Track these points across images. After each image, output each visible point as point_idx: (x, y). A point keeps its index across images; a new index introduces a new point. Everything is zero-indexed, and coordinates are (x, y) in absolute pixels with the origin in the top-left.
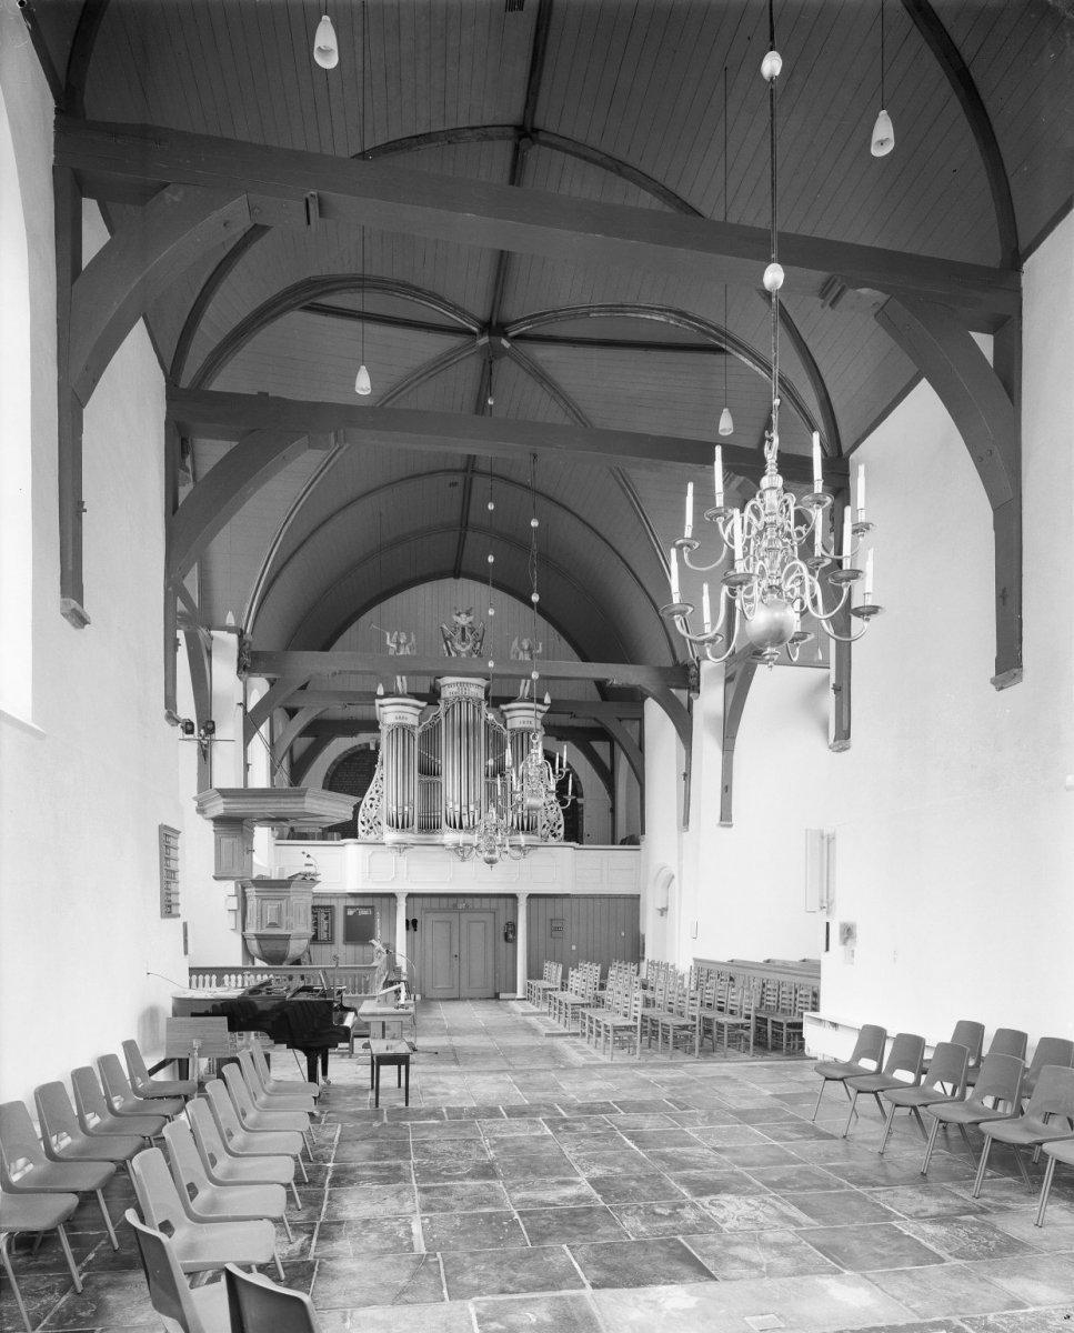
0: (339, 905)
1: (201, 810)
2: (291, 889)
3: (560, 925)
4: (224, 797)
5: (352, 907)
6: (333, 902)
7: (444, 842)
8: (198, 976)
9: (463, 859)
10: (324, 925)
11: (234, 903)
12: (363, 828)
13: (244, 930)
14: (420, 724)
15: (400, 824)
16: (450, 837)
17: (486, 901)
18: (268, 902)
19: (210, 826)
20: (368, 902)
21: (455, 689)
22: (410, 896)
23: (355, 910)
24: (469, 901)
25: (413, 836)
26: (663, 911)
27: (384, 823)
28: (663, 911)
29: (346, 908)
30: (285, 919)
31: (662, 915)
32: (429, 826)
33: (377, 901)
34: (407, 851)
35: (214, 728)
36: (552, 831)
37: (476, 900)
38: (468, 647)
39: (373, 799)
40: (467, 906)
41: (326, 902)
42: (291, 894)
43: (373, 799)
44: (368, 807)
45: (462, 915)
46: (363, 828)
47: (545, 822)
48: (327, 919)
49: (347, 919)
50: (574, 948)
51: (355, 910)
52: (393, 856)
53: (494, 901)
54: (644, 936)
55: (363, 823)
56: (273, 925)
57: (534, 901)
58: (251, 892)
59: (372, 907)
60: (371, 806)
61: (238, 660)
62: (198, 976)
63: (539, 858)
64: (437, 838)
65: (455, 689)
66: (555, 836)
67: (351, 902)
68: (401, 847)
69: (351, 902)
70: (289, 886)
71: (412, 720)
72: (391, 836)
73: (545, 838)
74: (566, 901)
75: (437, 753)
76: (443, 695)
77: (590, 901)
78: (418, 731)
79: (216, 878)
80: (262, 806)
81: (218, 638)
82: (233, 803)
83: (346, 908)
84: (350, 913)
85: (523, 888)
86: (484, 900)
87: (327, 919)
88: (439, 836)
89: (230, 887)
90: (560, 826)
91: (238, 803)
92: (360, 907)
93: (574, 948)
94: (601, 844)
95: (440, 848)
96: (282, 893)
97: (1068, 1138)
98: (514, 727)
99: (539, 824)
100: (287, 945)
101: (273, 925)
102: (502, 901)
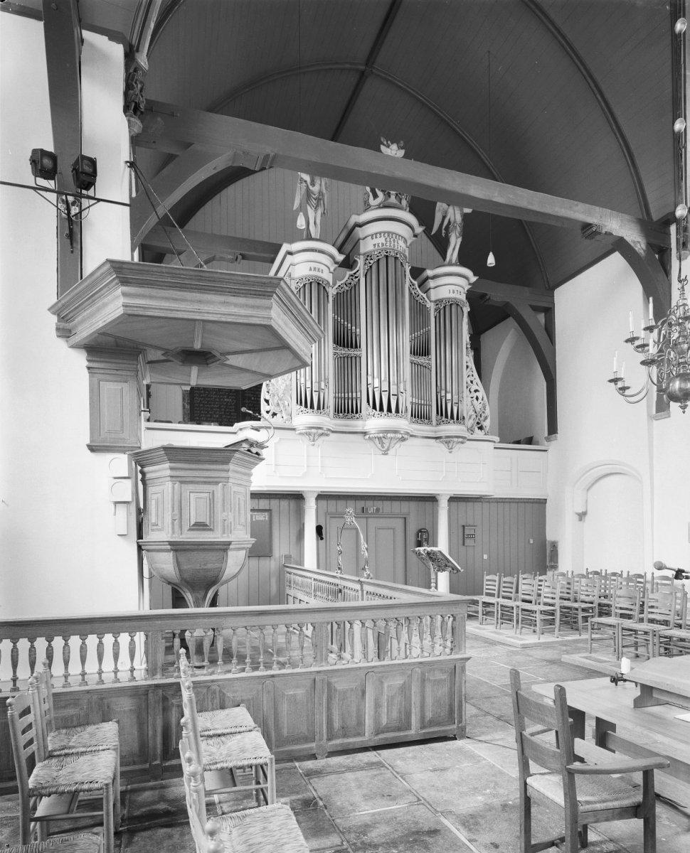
1: (65, 332)
2: (231, 466)
3: (473, 533)
4: (124, 282)
7: (366, 429)
8: (84, 637)
9: (385, 453)
11: (125, 491)
12: (268, 408)
13: (140, 536)
16: (374, 422)
17: (396, 504)
18: (191, 487)
19: (80, 360)
21: (381, 240)
24: (379, 504)
25: (328, 419)
26: (582, 516)
28: (582, 516)
30: (220, 516)
31: (581, 520)
32: (346, 409)
33: (275, 503)
35: (94, 174)
36: (478, 423)
37: (387, 503)
40: (378, 510)
42: (230, 474)
45: (370, 520)
50: (485, 557)
53: (405, 505)
54: (554, 545)
55: (267, 401)
56: (200, 526)
57: (454, 504)
58: (160, 471)
59: (269, 511)
61: (126, 94)
62: (84, 637)
63: (465, 452)
64: (358, 425)
65: (381, 240)
66: (481, 428)
68: (315, 433)
70: (226, 462)
71: (327, 276)
73: (471, 430)
74: (478, 505)
75: (354, 320)
76: (362, 250)
78: (332, 292)
79: (92, 448)
80: (196, 306)
81: (92, 46)
82: (97, 361)
85: (444, 487)
88: (359, 423)
89: (120, 463)
90: (486, 418)
91: (151, 297)
93: (485, 557)
95: (360, 437)
96: (213, 471)
98: (441, 297)
100: (223, 560)
101: (200, 526)
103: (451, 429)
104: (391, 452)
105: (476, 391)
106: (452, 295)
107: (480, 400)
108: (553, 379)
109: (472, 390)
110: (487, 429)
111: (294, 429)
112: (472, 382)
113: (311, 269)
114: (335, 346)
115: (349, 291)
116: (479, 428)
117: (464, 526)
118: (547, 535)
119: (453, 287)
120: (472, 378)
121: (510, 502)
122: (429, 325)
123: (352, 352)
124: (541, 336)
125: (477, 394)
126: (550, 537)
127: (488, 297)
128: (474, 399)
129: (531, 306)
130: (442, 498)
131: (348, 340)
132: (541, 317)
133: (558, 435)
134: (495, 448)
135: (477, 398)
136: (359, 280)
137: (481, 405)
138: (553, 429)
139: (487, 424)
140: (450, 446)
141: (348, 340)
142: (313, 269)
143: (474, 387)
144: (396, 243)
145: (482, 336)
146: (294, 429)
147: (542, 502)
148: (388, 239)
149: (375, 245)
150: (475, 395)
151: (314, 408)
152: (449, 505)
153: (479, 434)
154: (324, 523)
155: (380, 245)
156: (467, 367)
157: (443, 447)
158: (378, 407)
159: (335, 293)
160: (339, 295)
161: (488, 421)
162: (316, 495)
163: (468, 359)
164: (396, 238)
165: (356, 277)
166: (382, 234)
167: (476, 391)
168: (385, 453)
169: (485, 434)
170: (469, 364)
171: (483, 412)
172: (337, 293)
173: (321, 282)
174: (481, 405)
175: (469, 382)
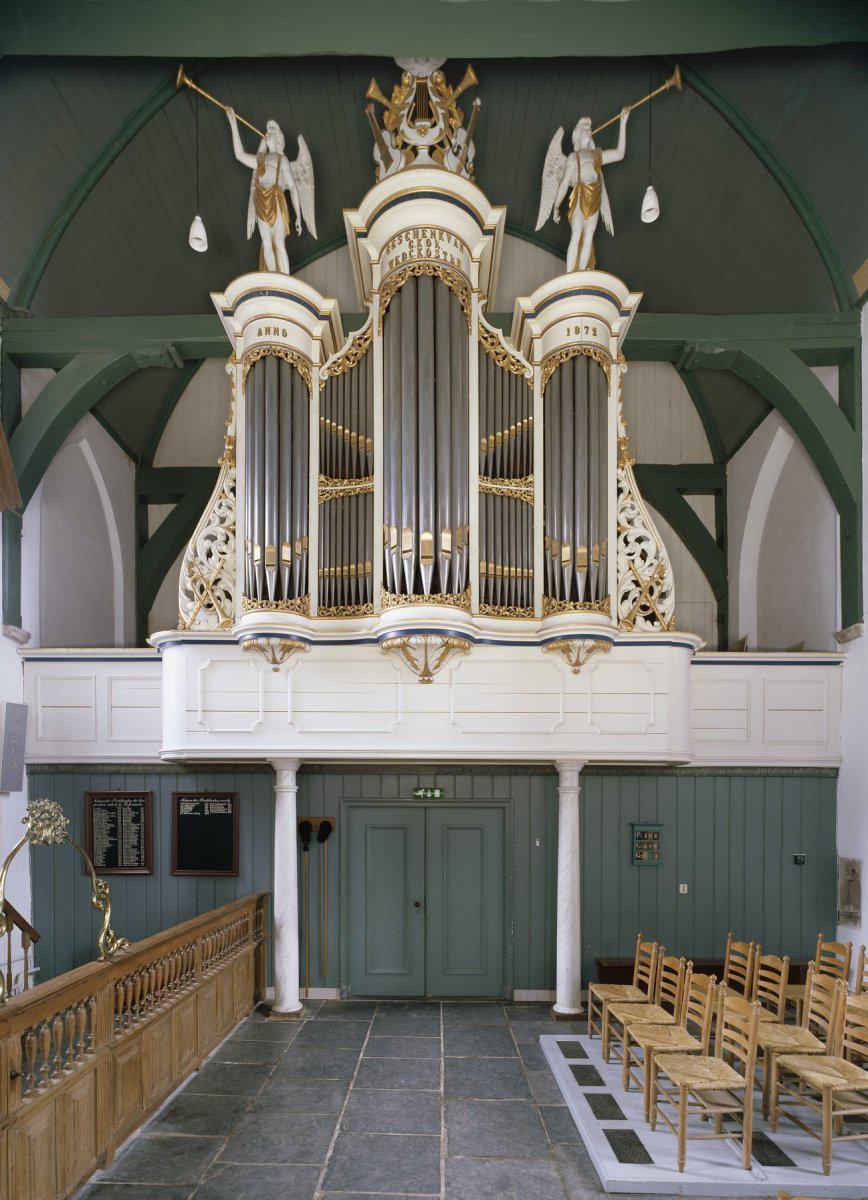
0: (164, 790)
5: (190, 796)
6: (151, 785)
10: (130, 835)
14: (324, 358)
15: (283, 591)
20: (225, 784)
22: (593, 772)
23: (196, 802)
27: (238, 593)
29: (178, 797)
32: (347, 596)
34: (293, 658)
38: (433, 136)
39: (212, 538)
41: (135, 785)
43: (212, 538)
44: (202, 557)
46: (190, 605)
47: (629, 586)
48: (136, 820)
49: (182, 824)
50: (683, 889)
51: (196, 802)
52: (255, 669)
53: (502, 783)
54: (854, 870)
60: (209, 554)
63: (613, 670)
64: (363, 626)
66: (652, 618)
67: (187, 784)
68: (278, 647)
69: (187, 784)
72: (251, 619)
77: (721, 782)
78: (317, 377)
83: (178, 797)
84: (187, 808)
86: (367, 778)
87: (136, 820)
88: (368, 621)
90: (663, 596)
92: (207, 795)
93: (683, 889)
94: (326, 765)
95: (372, 650)
97: (324, 782)
99: (612, 590)
102: (519, 783)
103: (574, 620)
104: (439, 677)
105: (639, 540)
106: (574, 339)
107: (650, 559)
108: (855, 504)
109: (631, 539)
110: (667, 619)
111: (236, 643)
112: (630, 522)
113: (260, 333)
114: (323, 478)
115: (355, 372)
116: (646, 618)
117: (632, 824)
118: (838, 840)
119: (576, 322)
120: (631, 514)
121: (745, 776)
122: (530, 412)
123: (355, 486)
124: (829, 426)
125: (644, 545)
126: (844, 850)
127: (687, 349)
128: (637, 557)
129: (799, 353)
130: (564, 768)
131: (522, 598)
132: (829, 378)
133: (864, 626)
134: (693, 663)
135: (644, 556)
136: (372, 342)
137: (653, 569)
138: (852, 612)
139: (667, 607)
140: (574, 660)
141: (522, 598)
142: (263, 331)
143: (633, 533)
144: (433, 248)
145: (729, 466)
146: (236, 643)
147: (826, 777)
148: (415, 244)
149: (391, 263)
150: (637, 548)
151: (268, 599)
152: (582, 784)
153: (645, 630)
154: (423, 900)
155: (400, 260)
156: (620, 491)
157: (558, 660)
158: (397, 588)
159: (326, 378)
160: (334, 379)
161: (670, 601)
162: (295, 767)
163: (622, 474)
164: (433, 234)
165: (366, 340)
166: (404, 235)
167: (639, 540)
168: (426, 676)
169: (662, 630)
170: (624, 484)
171: (658, 584)
172: (331, 378)
173: (282, 355)
174: (653, 569)
175: (624, 523)
